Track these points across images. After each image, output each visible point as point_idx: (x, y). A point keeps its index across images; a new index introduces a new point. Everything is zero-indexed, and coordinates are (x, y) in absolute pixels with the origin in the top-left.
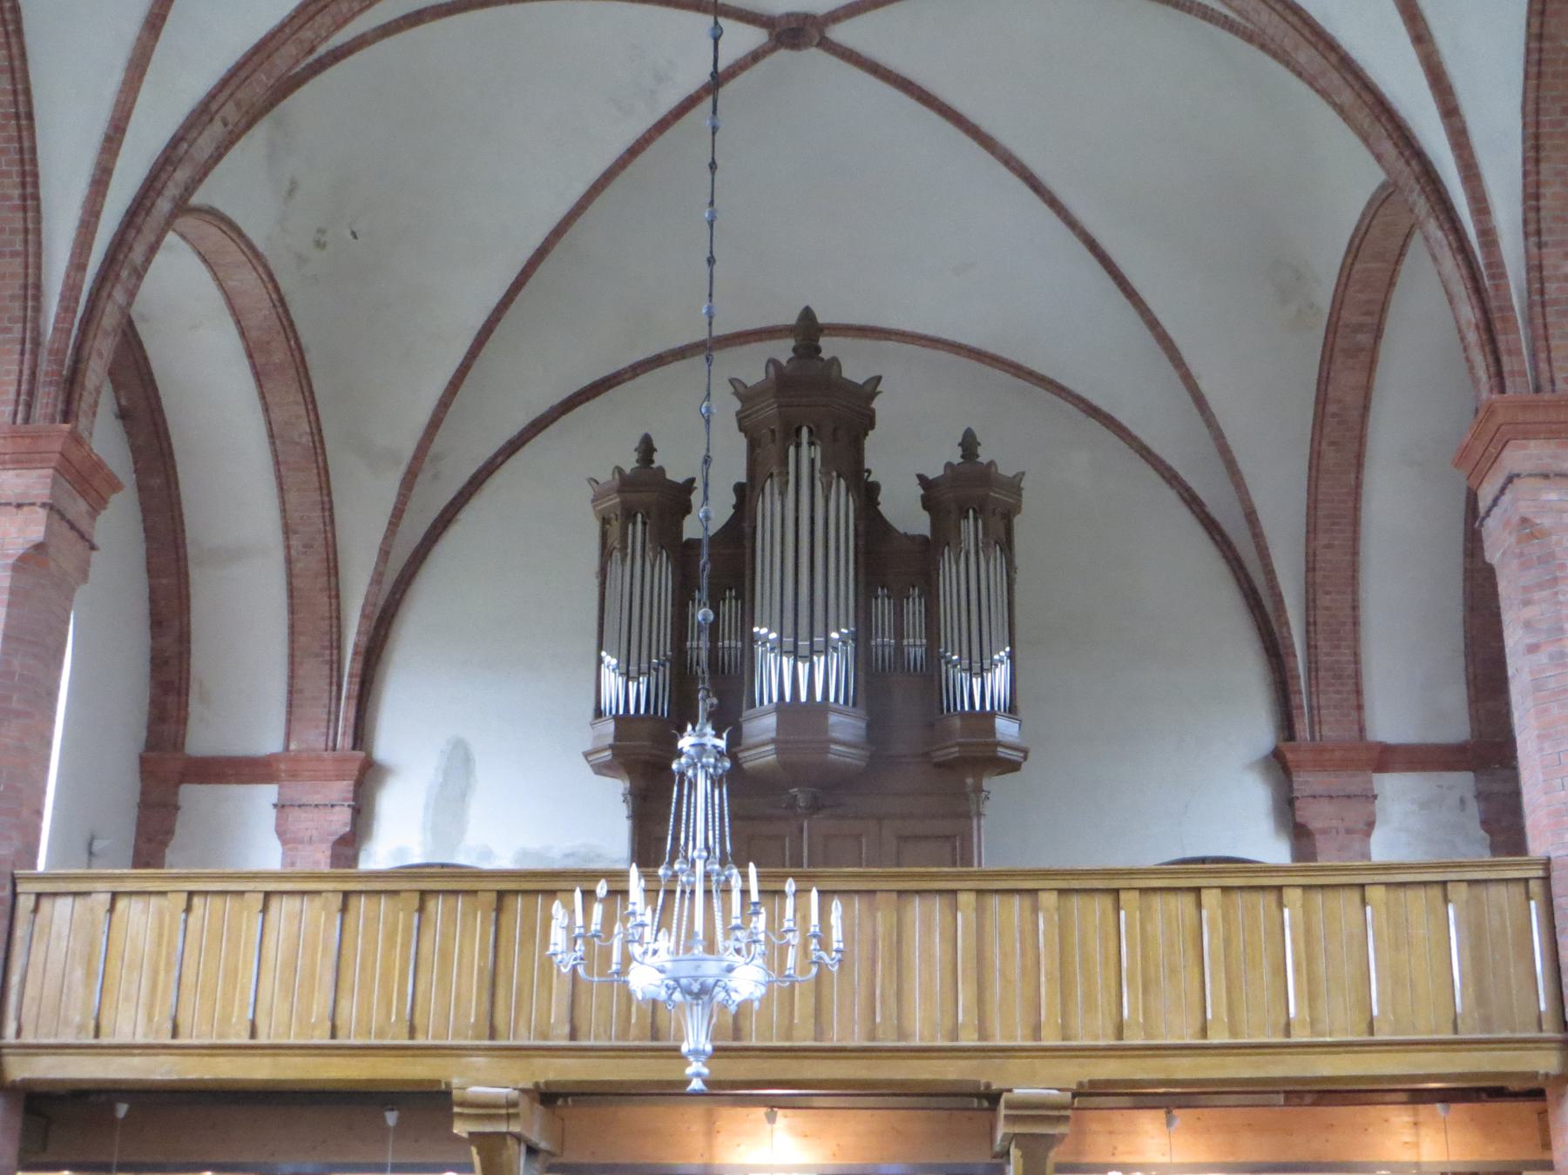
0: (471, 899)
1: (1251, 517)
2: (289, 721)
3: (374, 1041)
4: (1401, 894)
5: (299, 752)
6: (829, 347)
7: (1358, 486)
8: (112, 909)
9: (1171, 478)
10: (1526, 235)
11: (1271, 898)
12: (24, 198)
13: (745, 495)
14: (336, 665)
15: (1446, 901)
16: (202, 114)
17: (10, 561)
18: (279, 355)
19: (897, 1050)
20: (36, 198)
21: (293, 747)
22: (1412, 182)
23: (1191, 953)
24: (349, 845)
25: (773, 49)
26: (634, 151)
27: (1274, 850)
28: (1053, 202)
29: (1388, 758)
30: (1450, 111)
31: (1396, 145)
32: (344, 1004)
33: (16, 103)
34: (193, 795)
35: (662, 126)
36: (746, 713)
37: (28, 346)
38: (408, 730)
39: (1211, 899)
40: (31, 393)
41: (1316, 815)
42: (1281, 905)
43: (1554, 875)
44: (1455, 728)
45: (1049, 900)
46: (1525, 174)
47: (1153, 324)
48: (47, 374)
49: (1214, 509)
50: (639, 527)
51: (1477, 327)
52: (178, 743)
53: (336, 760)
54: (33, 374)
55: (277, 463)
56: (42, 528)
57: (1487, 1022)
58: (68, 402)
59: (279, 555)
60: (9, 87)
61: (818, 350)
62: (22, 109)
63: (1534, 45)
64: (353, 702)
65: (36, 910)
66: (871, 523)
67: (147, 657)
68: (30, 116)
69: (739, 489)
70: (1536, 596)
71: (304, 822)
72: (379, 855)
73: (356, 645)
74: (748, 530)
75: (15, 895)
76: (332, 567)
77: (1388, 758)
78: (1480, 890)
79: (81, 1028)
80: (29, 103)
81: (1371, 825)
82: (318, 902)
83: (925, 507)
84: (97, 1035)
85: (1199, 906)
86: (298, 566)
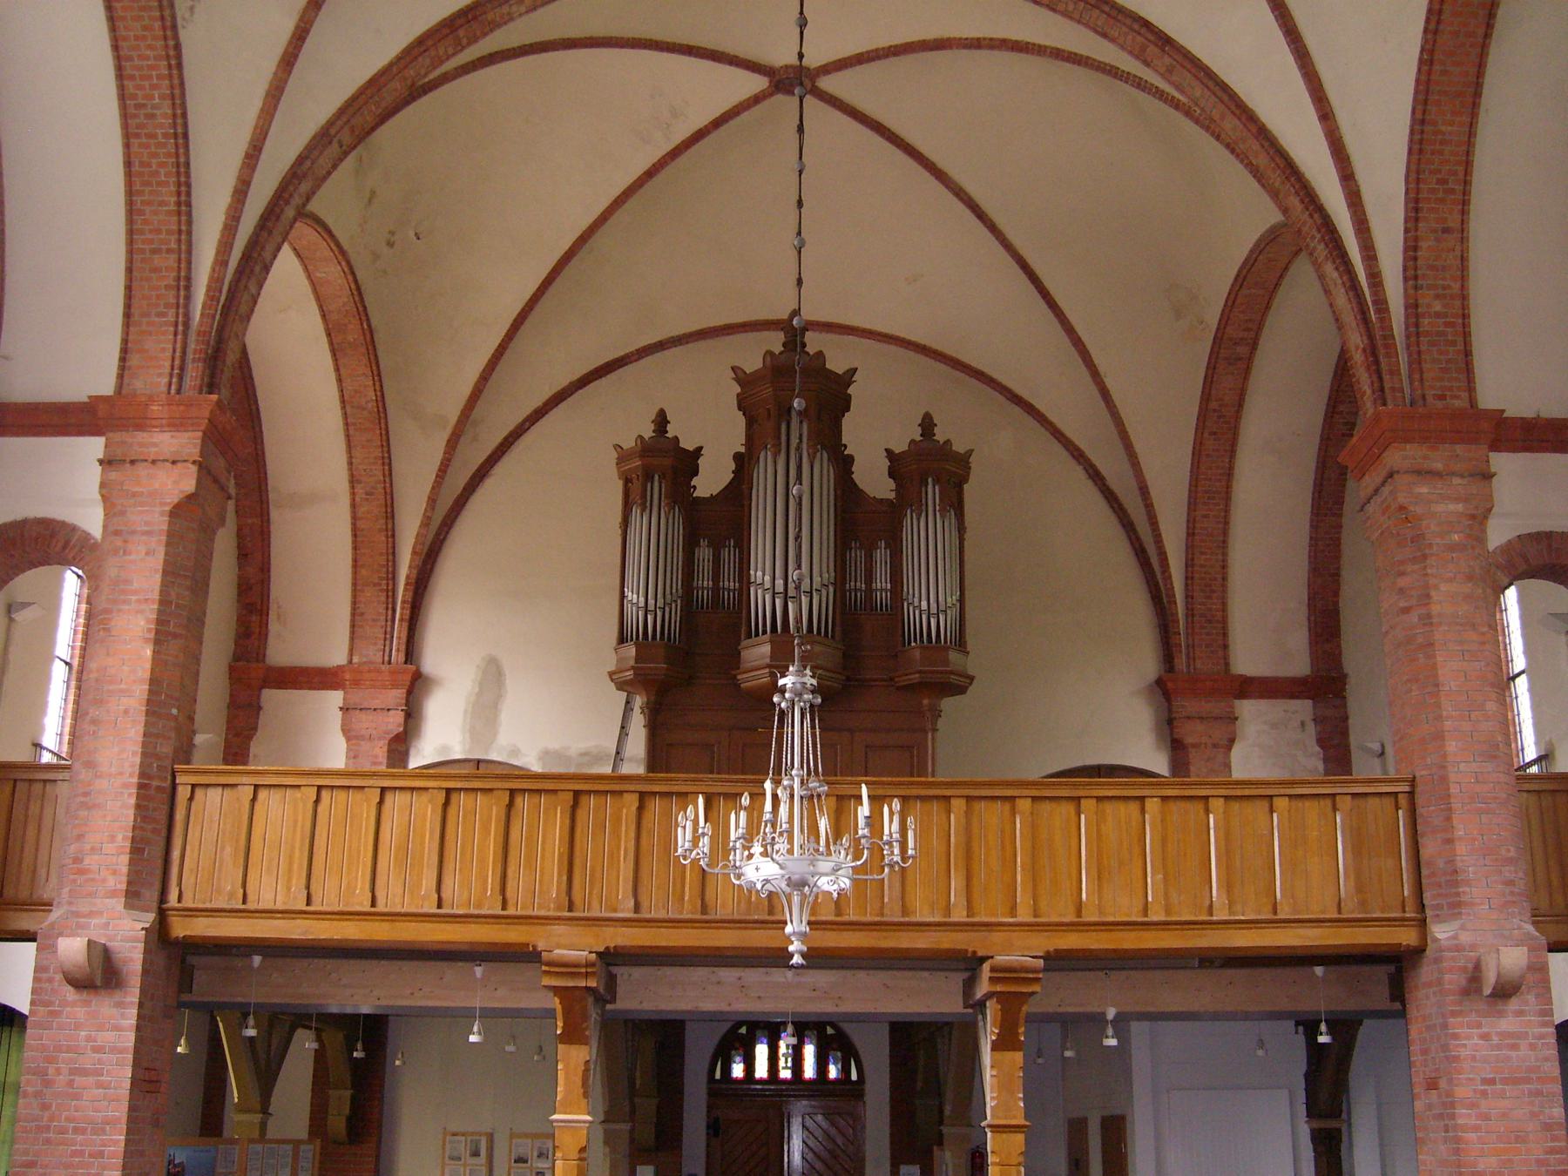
0: (553, 797)
1: (1144, 491)
2: (352, 639)
3: (473, 911)
4: (1299, 804)
5: (360, 664)
6: (813, 342)
7: (1231, 468)
8: (254, 799)
9: (1078, 455)
10: (1406, 279)
11: (1200, 806)
12: (179, 204)
13: (744, 464)
14: (391, 593)
15: (1335, 809)
16: (324, 137)
17: (168, 508)
18: (353, 334)
19: (901, 924)
20: (189, 204)
21: (355, 660)
22: (1314, 232)
23: (1137, 850)
24: (400, 745)
25: (771, 95)
26: (650, 174)
27: (1159, 763)
28: (993, 228)
29: (1249, 687)
30: (1347, 177)
31: (1302, 201)
32: (448, 882)
33: (175, 126)
34: (272, 698)
35: (675, 154)
36: (744, 643)
37: (180, 328)
38: (452, 652)
39: (1152, 805)
40: (182, 368)
41: (1192, 733)
42: (1207, 812)
43: (1418, 790)
44: (1299, 665)
45: (1024, 805)
46: (1406, 231)
47: (1070, 330)
48: (195, 351)
49: (1113, 483)
50: (656, 484)
51: (1364, 350)
52: (260, 656)
53: (392, 673)
54: (184, 353)
55: (347, 424)
56: (194, 482)
57: (1363, 904)
58: (212, 376)
59: (345, 501)
60: (169, 112)
61: (804, 345)
62: (180, 130)
63: (1417, 127)
64: (405, 625)
65: (191, 799)
66: (847, 491)
67: (235, 584)
68: (186, 136)
69: (738, 457)
70: (1409, 568)
71: (364, 722)
72: (424, 754)
73: (408, 577)
74: (746, 492)
75: (174, 786)
76: (390, 514)
77: (1249, 687)
78: (1360, 802)
79: (231, 895)
80: (185, 125)
81: (1232, 741)
82: (425, 797)
83: (891, 475)
84: (244, 902)
85: (1143, 811)
86: (361, 511)
